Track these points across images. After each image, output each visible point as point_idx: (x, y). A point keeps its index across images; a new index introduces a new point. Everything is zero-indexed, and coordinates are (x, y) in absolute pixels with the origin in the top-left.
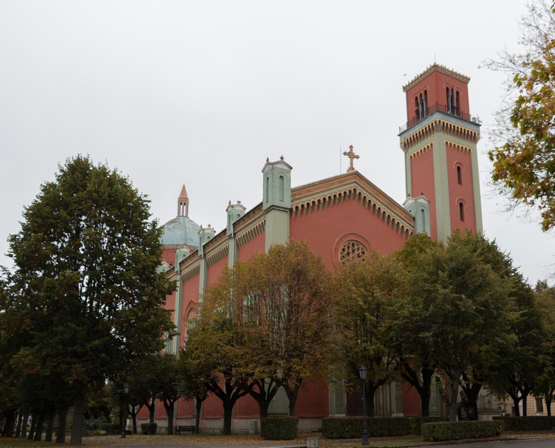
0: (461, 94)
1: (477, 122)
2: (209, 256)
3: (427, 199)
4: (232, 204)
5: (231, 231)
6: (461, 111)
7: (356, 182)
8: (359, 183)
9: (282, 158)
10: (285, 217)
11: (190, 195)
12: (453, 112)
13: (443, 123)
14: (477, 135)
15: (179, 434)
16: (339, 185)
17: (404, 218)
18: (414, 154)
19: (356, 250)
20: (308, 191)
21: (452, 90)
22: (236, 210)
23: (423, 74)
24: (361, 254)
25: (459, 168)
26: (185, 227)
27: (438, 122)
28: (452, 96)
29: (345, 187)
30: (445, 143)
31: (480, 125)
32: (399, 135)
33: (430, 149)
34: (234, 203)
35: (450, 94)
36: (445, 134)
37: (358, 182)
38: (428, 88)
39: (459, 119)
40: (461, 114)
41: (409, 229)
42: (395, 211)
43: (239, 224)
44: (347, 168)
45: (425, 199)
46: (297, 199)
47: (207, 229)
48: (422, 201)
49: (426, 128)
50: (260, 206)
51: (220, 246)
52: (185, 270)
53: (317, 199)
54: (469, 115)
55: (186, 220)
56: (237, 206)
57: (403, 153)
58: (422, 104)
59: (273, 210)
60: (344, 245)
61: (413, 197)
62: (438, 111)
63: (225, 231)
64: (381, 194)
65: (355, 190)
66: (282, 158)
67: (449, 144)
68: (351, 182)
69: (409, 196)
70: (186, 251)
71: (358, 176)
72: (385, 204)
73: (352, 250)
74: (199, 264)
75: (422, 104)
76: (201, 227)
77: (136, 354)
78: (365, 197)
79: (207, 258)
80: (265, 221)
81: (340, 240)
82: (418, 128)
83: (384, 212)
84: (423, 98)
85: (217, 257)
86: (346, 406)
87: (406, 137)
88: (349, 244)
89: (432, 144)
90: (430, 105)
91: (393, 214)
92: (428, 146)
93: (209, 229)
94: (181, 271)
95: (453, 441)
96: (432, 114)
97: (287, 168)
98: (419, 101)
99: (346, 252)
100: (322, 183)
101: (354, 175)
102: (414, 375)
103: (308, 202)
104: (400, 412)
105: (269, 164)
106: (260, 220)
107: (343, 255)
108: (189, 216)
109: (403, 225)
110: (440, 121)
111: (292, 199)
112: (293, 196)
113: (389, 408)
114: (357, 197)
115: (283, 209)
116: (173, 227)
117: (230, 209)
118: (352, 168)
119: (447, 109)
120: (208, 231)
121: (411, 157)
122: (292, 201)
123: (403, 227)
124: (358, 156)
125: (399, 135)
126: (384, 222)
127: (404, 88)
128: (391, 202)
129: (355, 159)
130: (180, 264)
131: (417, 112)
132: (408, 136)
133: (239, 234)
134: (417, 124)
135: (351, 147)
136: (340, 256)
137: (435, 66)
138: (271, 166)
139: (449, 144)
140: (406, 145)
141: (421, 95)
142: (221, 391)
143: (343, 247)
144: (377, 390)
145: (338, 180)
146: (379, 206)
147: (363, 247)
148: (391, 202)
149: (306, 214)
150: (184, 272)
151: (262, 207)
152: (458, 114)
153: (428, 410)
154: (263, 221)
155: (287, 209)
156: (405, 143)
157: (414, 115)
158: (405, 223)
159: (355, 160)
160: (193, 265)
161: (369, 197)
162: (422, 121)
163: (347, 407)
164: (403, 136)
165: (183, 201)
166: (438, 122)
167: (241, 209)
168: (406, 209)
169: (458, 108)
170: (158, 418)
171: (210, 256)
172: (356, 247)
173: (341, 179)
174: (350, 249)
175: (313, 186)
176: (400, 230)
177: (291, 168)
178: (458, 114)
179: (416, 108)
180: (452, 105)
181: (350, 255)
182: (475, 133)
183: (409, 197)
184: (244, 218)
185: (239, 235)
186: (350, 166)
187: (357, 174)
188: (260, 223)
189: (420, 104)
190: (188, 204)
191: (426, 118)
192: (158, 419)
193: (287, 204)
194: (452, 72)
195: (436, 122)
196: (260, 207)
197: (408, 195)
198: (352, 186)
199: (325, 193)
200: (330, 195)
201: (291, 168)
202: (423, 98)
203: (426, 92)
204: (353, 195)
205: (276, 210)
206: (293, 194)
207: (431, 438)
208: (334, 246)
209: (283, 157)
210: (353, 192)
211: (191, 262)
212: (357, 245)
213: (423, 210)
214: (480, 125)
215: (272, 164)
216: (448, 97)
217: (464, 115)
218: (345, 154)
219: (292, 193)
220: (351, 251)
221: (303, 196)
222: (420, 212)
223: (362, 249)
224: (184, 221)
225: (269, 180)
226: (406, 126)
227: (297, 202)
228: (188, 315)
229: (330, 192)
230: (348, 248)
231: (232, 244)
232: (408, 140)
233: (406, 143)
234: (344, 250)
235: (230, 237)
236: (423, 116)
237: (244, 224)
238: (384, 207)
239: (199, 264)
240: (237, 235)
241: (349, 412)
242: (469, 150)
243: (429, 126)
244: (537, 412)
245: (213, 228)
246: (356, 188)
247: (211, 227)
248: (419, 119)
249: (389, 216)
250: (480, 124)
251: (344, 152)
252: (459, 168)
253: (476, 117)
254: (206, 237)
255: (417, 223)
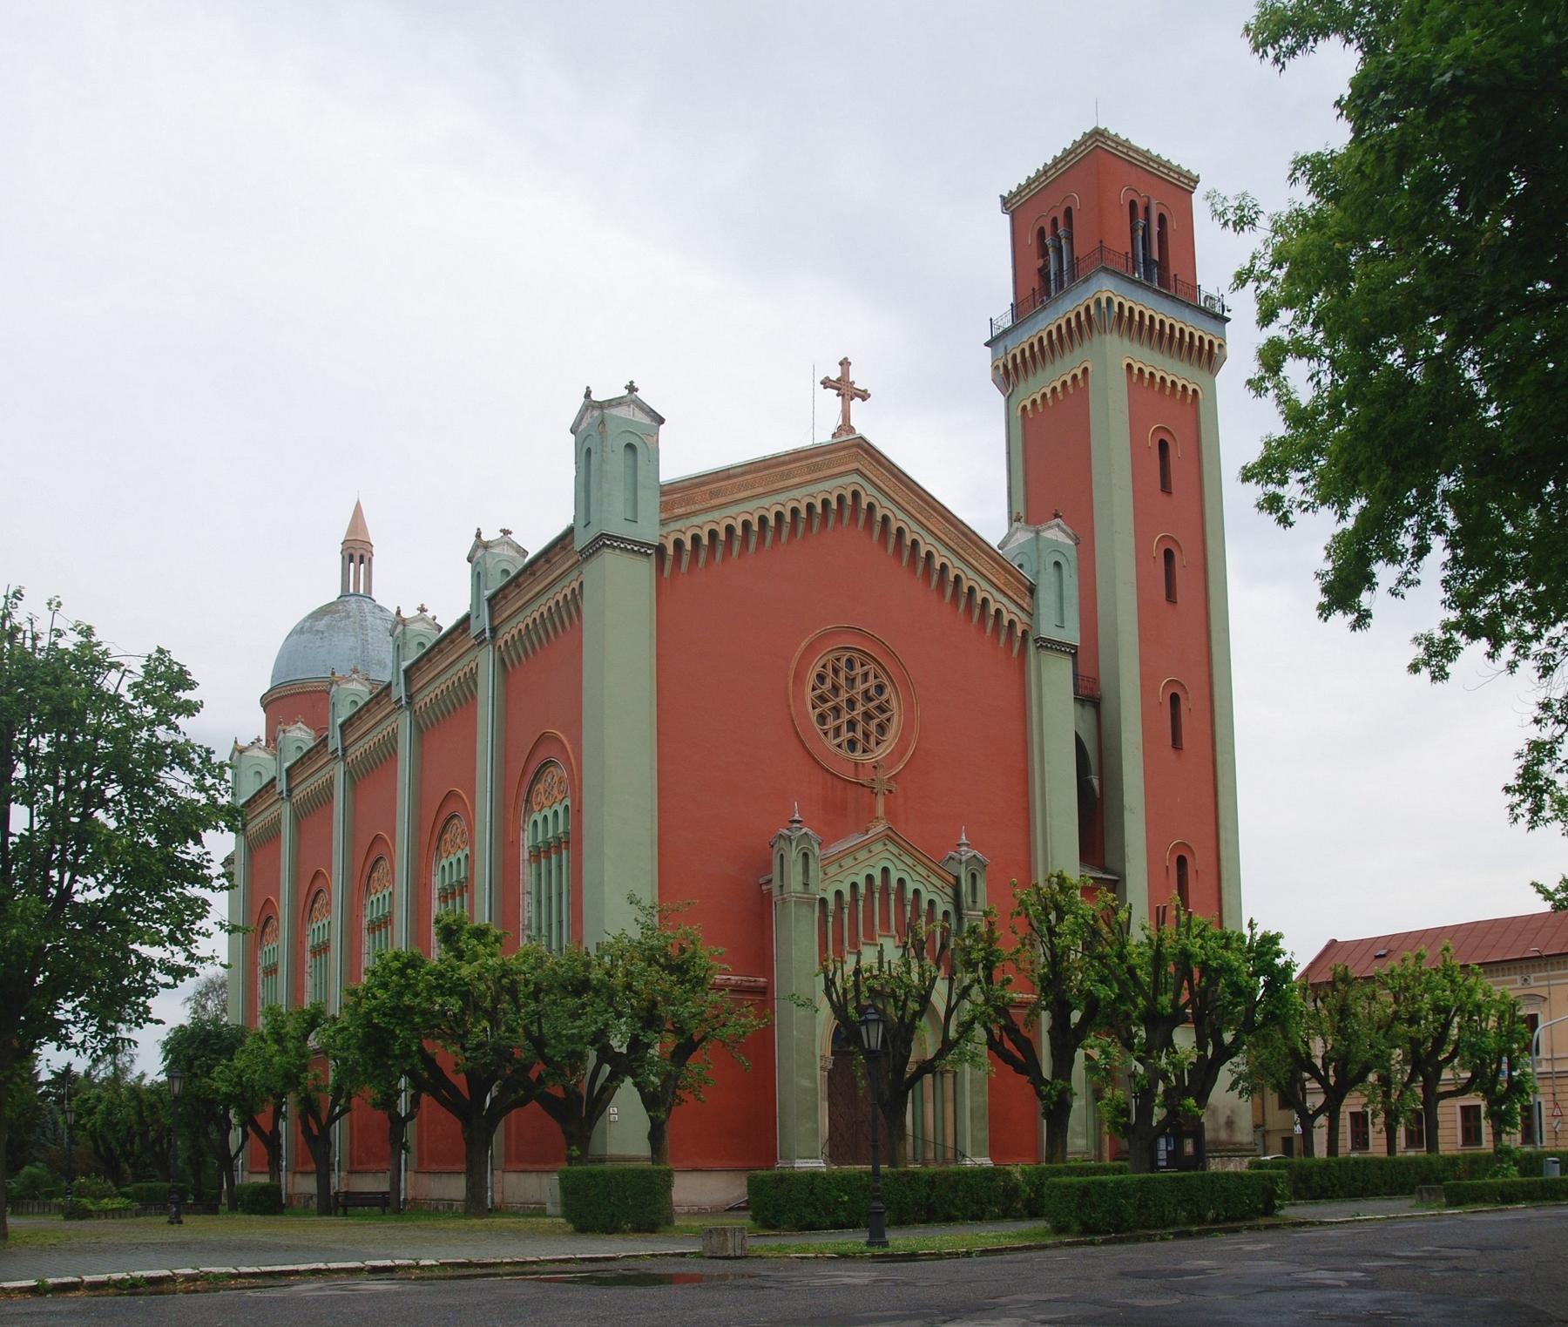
0: (1173, 225)
1: (1218, 310)
2: (424, 699)
3: (1070, 531)
4: (485, 538)
5: (483, 622)
6: (1172, 275)
7: (857, 471)
8: (868, 473)
9: (631, 388)
10: (644, 570)
11: (376, 534)
12: (1148, 276)
13: (1121, 305)
14: (1216, 350)
15: (345, 1214)
16: (809, 477)
17: (1000, 585)
18: (1034, 402)
19: (859, 680)
20: (714, 494)
21: (1147, 209)
22: (498, 555)
23: (1062, 159)
24: (872, 692)
25: (1163, 446)
26: (362, 627)
27: (1104, 304)
28: (1146, 228)
29: (827, 485)
30: (1124, 367)
31: (1228, 320)
32: (987, 344)
33: (1081, 384)
34: (489, 535)
35: (1141, 222)
36: (1126, 341)
37: (865, 471)
38: (1077, 203)
39: (1167, 296)
40: (1172, 283)
41: (1016, 619)
42: (976, 564)
43: (505, 597)
44: (833, 429)
45: (1064, 531)
46: (679, 517)
47: (414, 620)
48: (1055, 534)
49: (1069, 321)
50: (564, 541)
51: (452, 671)
52: (356, 747)
53: (740, 520)
54: (1195, 288)
55: (367, 606)
56: (498, 543)
57: (1000, 399)
58: (1059, 251)
59: (605, 550)
60: (822, 663)
61: (1027, 522)
62: (1106, 270)
63: (464, 623)
64: (935, 510)
65: (855, 494)
66: (631, 388)
67: (1136, 371)
68: (842, 469)
69: (1019, 520)
70: (358, 690)
71: (866, 451)
72: (947, 540)
73: (847, 678)
74: (394, 725)
75: (1059, 251)
76: (398, 613)
77: (47, 974)
78: (885, 519)
79: (417, 707)
80: (581, 584)
81: (811, 649)
82: (1047, 322)
83: (943, 566)
84: (1061, 231)
85: (445, 702)
86: (827, 1135)
87: (1009, 348)
88: (838, 660)
89: (1085, 370)
90: (1079, 251)
91: (971, 574)
92: (1075, 377)
93: (423, 619)
94: (345, 750)
95: (1140, 1232)
96: (1086, 280)
97: (647, 420)
98: (1048, 241)
99: (829, 682)
100: (756, 471)
101: (854, 450)
102: (1028, 1047)
103: (714, 526)
104: (981, 1156)
105: (593, 407)
106: (565, 582)
107: (819, 691)
108: (373, 596)
109: (998, 606)
110: (1109, 301)
111: (664, 516)
112: (665, 506)
113: (950, 1143)
114: (862, 518)
115: (637, 548)
116: (329, 627)
117: (480, 553)
118: (846, 427)
119: (1130, 265)
120: (418, 627)
121: (1024, 408)
122: (663, 523)
123: (998, 612)
124: (865, 391)
125: (987, 344)
126: (944, 597)
127: (1006, 202)
128: (965, 535)
129: (857, 400)
130: (344, 727)
131: (1043, 273)
132: (1015, 345)
133: (505, 628)
134: (1044, 308)
135: (845, 364)
136: (809, 695)
137: (1098, 134)
138: (596, 413)
139: (1136, 371)
140: (1009, 375)
141: (1055, 221)
142: (453, 1089)
143: (818, 669)
144: (918, 1085)
145: (804, 463)
146: (929, 548)
147: (880, 672)
148: (965, 535)
149: (708, 563)
150: (355, 752)
151: (572, 542)
152: (1163, 282)
153: (1065, 1145)
154: (575, 585)
155: (650, 546)
156: (1005, 366)
157: (1035, 282)
158: (1005, 600)
159: (856, 403)
160: (379, 729)
161: (898, 519)
162: (1056, 299)
163: (830, 1138)
164: (1001, 346)
165: (356, 553)
166: (1104, 304)
167: (512, 553)
168: (1009, 558)
169: (1163, 265)
170: (301, 1169)
171: (424, 699)
172: (858, 670)
173: (814, 460)
174: (842, 675)
175: (729, 477)
176: (990, 623)
177: (661, 421)
178: (1163, 282)
179: (1040, 263)
180: (1144, 255)
181: (842, 692)
182: (1211, 342)
183: (1016, 525)
184: (521, 579)
185: (508, 633)
186: (840, 423)
187: (865, 449)
188: (568, 591)
189: (1050, 250)
190: (370, 560)
191: (1069, 291)
192: (301, 1173)
193: (649, 530)
194: (1146, 154)
195: (1098, 302)
196: (567, 541)
197: (1013, 518)
198: (846, 484)
199: (766, 502)
200: (779, 508)
201: (661, 421)
202: (1061, 231)
203: (1068, 212)
204: (849, 509)
205: (615, 548)
206: (666, 502)
207: (1076, 1227)
208: (793, 665)
209: (635, 385)
210: (849, 501)
211: (373, 722)
212: (862, 665)
213: (1057, 564)
214: (1228, 320)
215: (601, 405)
216: (1133, 231)
217: (1179, 286)
218: (826, 383)
219: (664, 499)
220: (842, 681)
221: (698, 507)
222: (1051, 569)
223: (876, 677)
224: (361, 610)
225: (594, 457)
226: (1010, 317)
227: (679, 525)
228: (370, 877)
229: (782, 498)
230: (836, 671)
231: (485, 661)
232: (1014, 357)
233: (1010, 366)
234: (821, 678)
235: (480, 640)
236: (1060, 286)
237: (521, 598)
238: (944, 551)
239: (394, 725)
240: (417, 699)
241: (834, 1155)
242: (1195, 391)
243: (1078, 315)
244: (1353, 1149)
245: (434, 618)
246: (859, 489)
247: (429, 615)
248: (1049, 295)
249: (957, 578)
250: (1226, 314)
251: (822, 378)
252: (1163, 446)
253: (1215, 294)
254: (413, 645)
255: (1041, 603)
